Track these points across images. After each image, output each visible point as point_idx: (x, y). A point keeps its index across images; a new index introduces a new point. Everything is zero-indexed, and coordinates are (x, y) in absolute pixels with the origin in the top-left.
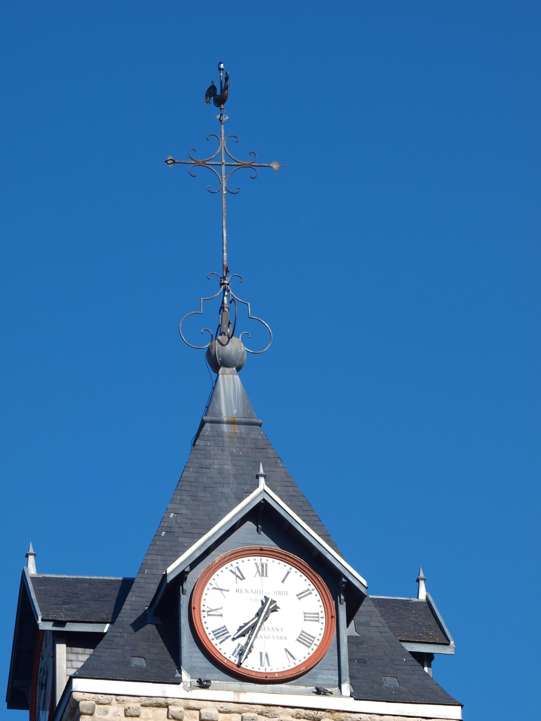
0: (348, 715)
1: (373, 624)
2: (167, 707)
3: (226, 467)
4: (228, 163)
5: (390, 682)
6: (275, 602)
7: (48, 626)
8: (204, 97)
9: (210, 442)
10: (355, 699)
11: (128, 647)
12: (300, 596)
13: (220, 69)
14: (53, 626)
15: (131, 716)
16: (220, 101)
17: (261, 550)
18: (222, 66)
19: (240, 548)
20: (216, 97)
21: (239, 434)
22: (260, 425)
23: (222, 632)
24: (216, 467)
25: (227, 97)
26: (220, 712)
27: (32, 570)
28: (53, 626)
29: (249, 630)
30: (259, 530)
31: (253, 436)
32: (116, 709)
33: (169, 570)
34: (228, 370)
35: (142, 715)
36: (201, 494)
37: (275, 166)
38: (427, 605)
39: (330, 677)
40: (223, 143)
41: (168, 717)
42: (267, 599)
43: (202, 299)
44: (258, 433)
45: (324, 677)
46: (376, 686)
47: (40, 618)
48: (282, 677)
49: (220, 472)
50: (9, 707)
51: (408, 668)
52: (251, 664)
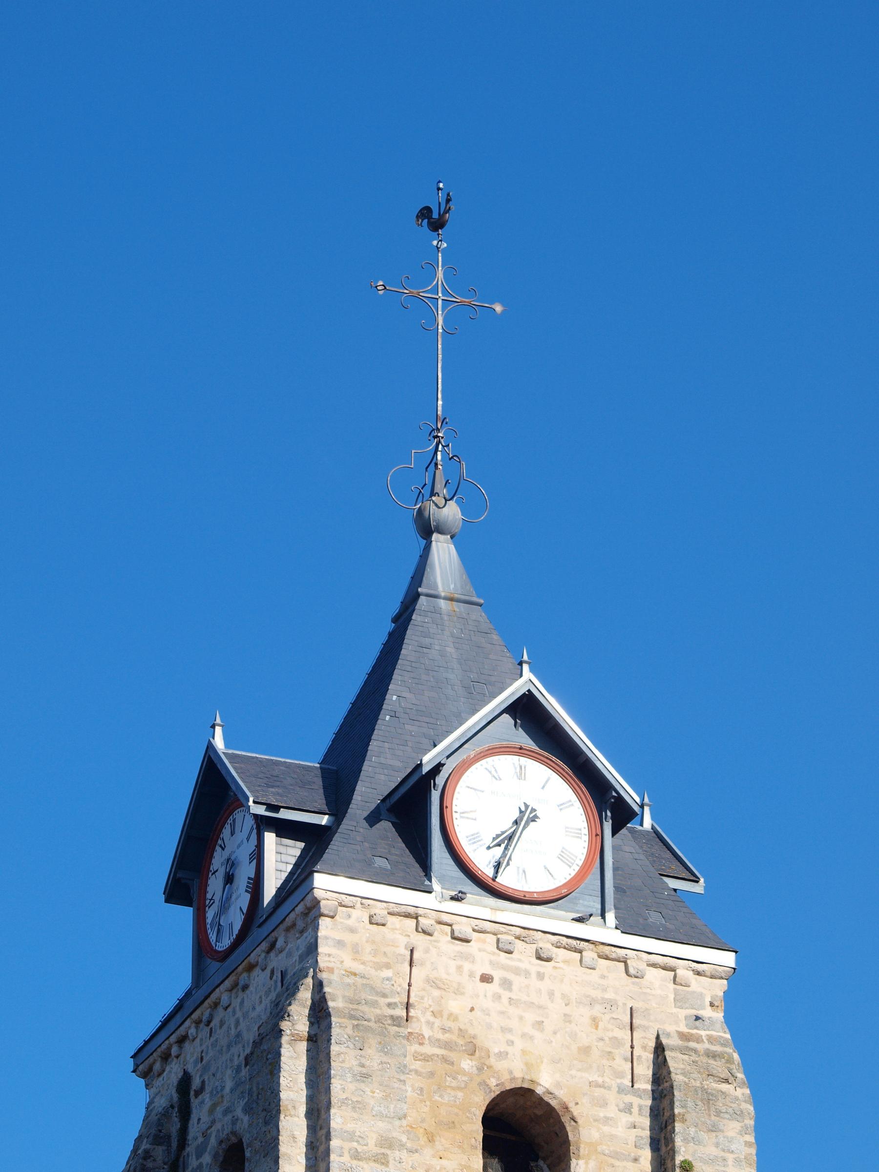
0: (613, 949)
1: (627, 849)
2: (416, 918)
3: (448, 649)
5: (654, 918)
6: (535, 810)
7: (261, 810)
10: (622, 932)
11: (366, 844)
12: (561, 806)
13: (439, 189)
14: (266, 810)
15: (377, 924)
17: (521, 748)
18: (441, 185)
19: (497, 744)
23: (475, 838)
24: (437, 647)
26: (474, 930)
27: (219, 742)
28: (266, 810)
29: (508, 840)
30: (518, 725)
31: (474, 617)
32: (359, 915)
33: (425, 759)
34: (442, 537)
35: (389, 925)
36: (424, 677)
37: (498, 308)
38: (654, 835)
39: (592, 904)
40: (440, 274)
41: (417, 930)
42: (527, 806)
45: (586, 903)
46: (641, 920)
47: (251, 799)
48: (542, 898)
49: (443, 654)
50: (167, 901)
51: (670, 902)
52: (507, 880)
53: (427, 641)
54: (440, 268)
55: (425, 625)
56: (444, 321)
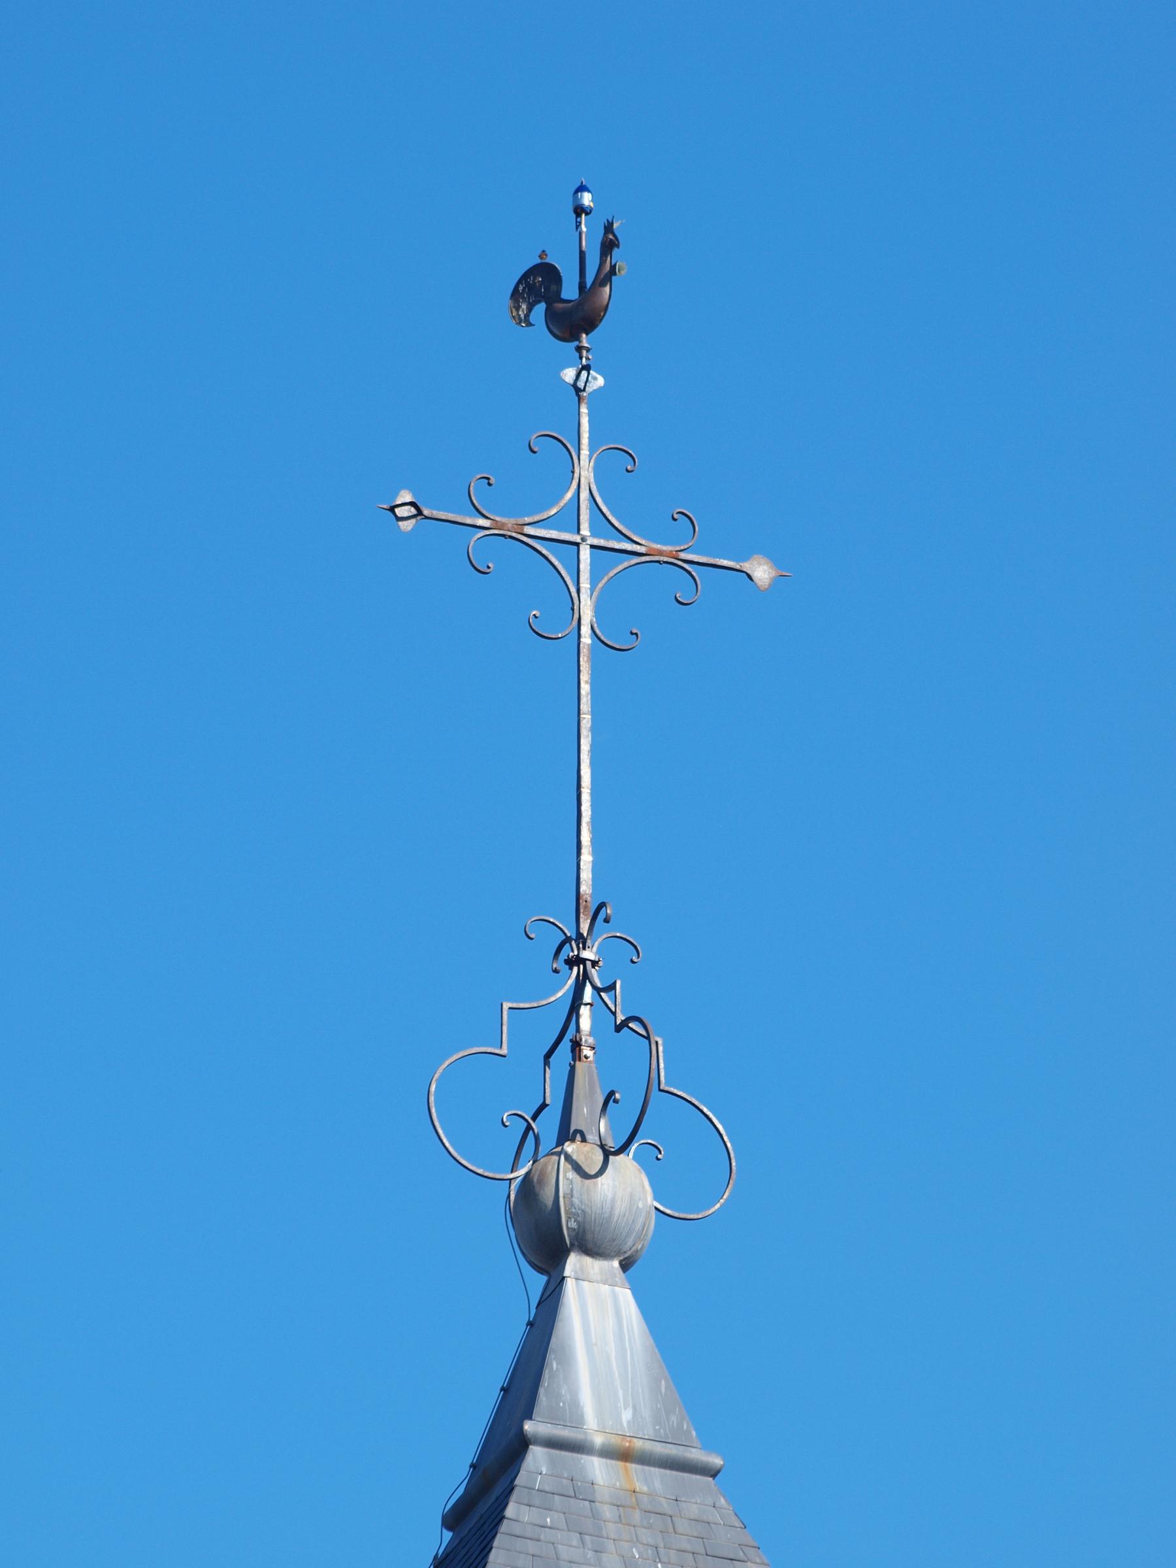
4: (602, 543)
8: (507, 302)
9: (556, 1515)
13: (579, 210)
16: (574, 322)
18: (587, 199)
21: (645, 1499)
22: (714, 1473)
31: (693, 1509)
34: (594, 1266)
37: (762, 572)
40: (586, 470)
43: (506, 1006)
44: (709, 1501)
55: (545, 1535)
56: (598, 610)
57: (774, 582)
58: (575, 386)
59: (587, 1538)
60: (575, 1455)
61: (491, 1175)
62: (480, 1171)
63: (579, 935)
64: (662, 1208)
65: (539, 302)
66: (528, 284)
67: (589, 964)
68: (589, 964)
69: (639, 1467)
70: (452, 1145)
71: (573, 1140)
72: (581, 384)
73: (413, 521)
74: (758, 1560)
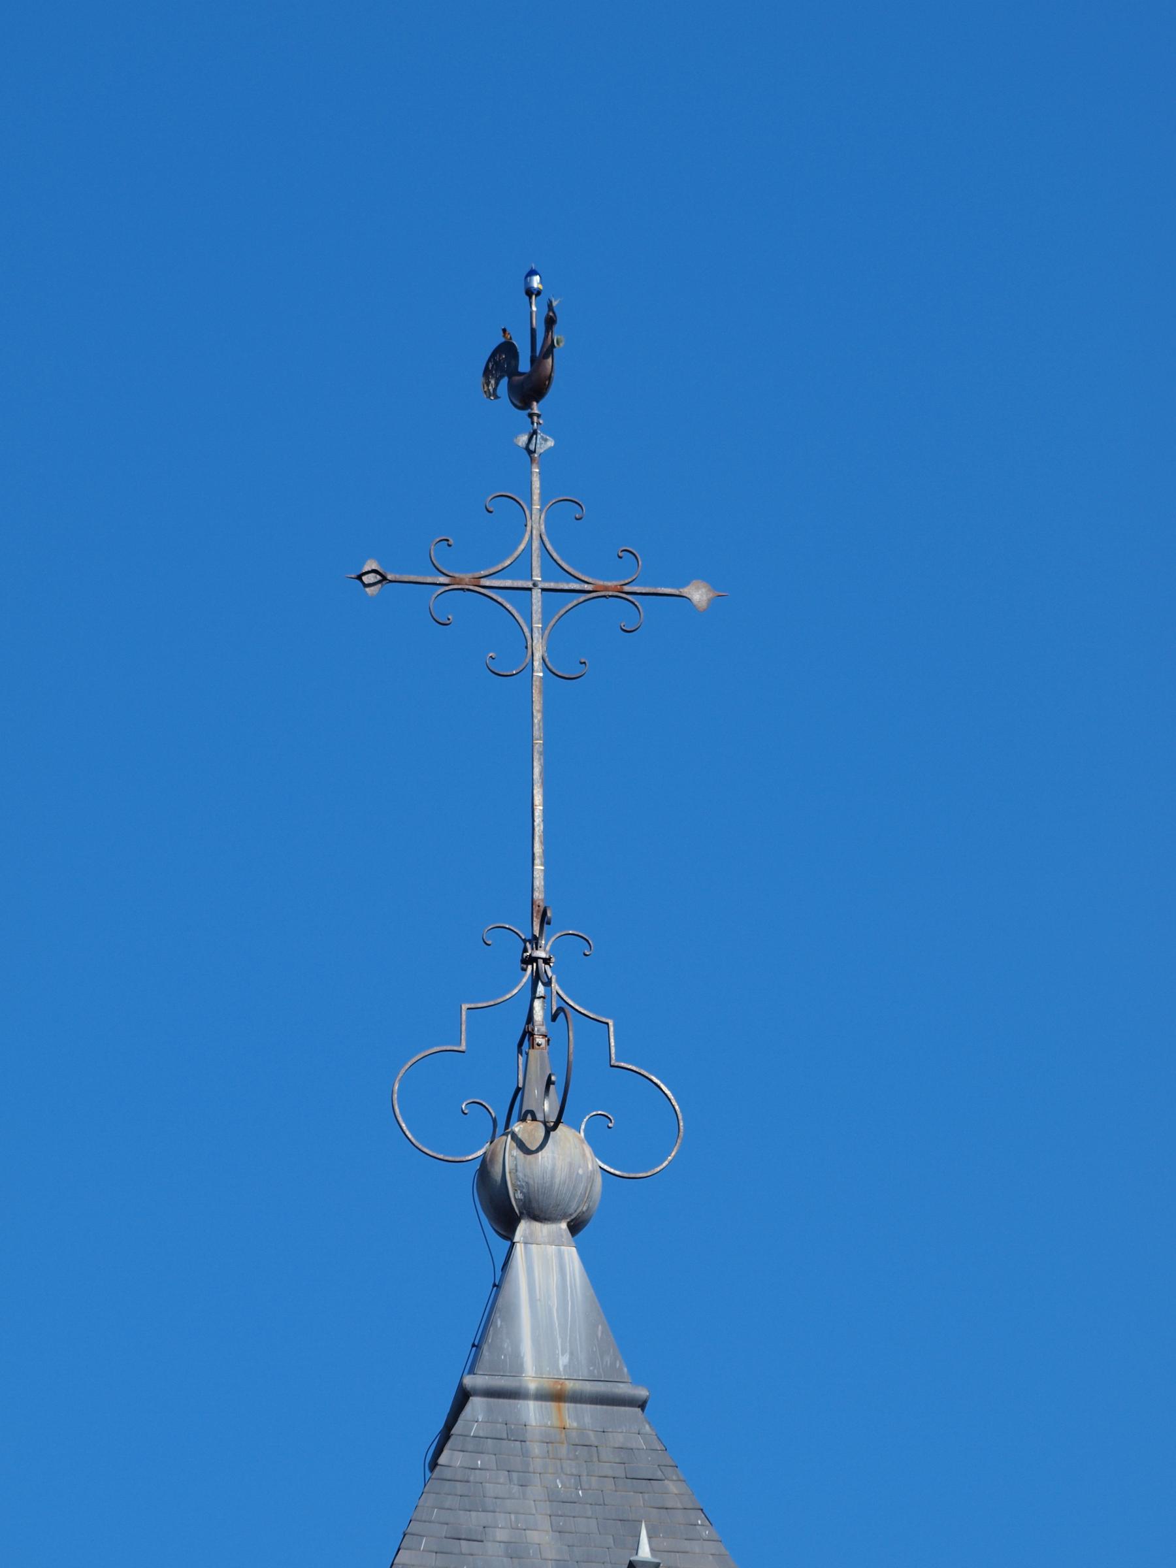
3: (534, 1536)
4: (552, 585)
8: (482, 380)
9: (486, 1457)
13: (530, 292)
16: (530, 391)
18: (536, 282)
20: (516, 378)
22: (642, 1405)
25: (550, 378)
31: (618, 1439)
37: (698, 594)
40: (537, 522)
43: (464, 1007)
53: (475, 1519)
54: (536, 507)
55: (474, 1476)
56: (550, 647)
57: (711, 602)
58: (527, 448)
59: (515, 1475)
60: (512, 1401)
61: (450, 1159)
62: (441, 1156)
63: (534, 937)
64: (605, 1167)
65: (501, 377)
66: (496, 363)
67: (540, 961)
68: (540, 961)
69: (572, 1405)
70: (413, 1135)
71: (523, 1119)
72: (532, 447)
73: (379, 586)
74: (674, 1478)
